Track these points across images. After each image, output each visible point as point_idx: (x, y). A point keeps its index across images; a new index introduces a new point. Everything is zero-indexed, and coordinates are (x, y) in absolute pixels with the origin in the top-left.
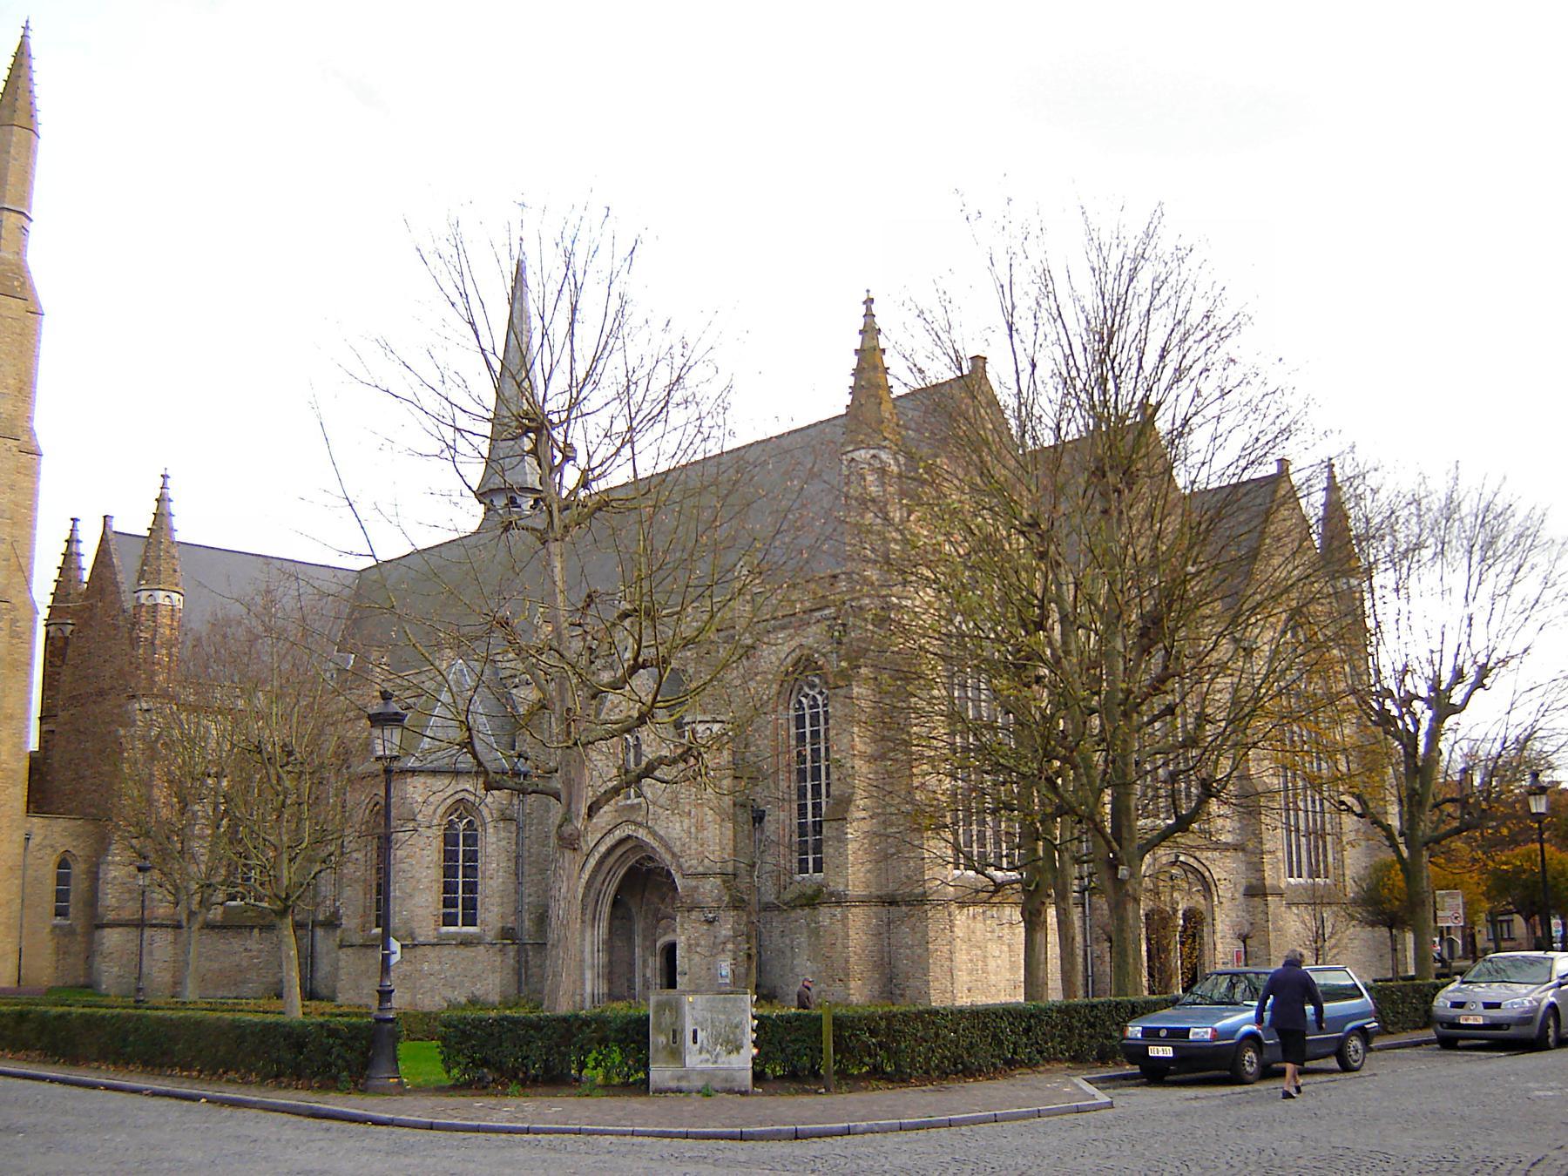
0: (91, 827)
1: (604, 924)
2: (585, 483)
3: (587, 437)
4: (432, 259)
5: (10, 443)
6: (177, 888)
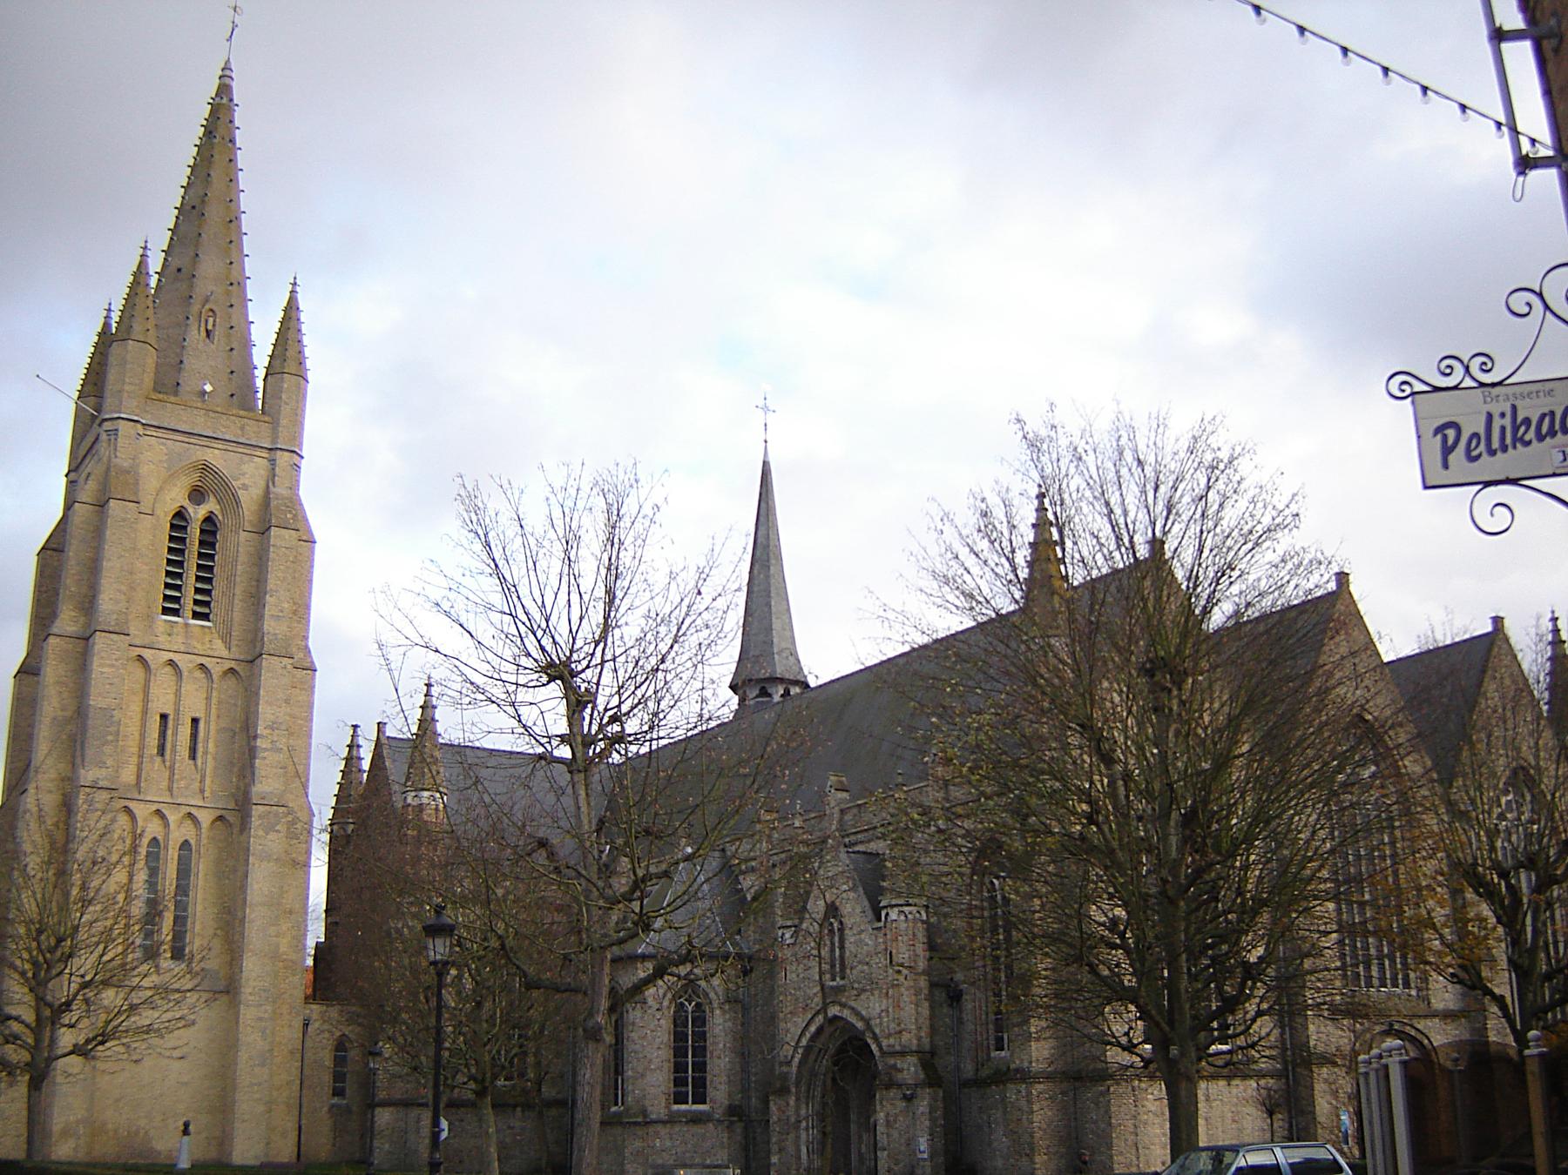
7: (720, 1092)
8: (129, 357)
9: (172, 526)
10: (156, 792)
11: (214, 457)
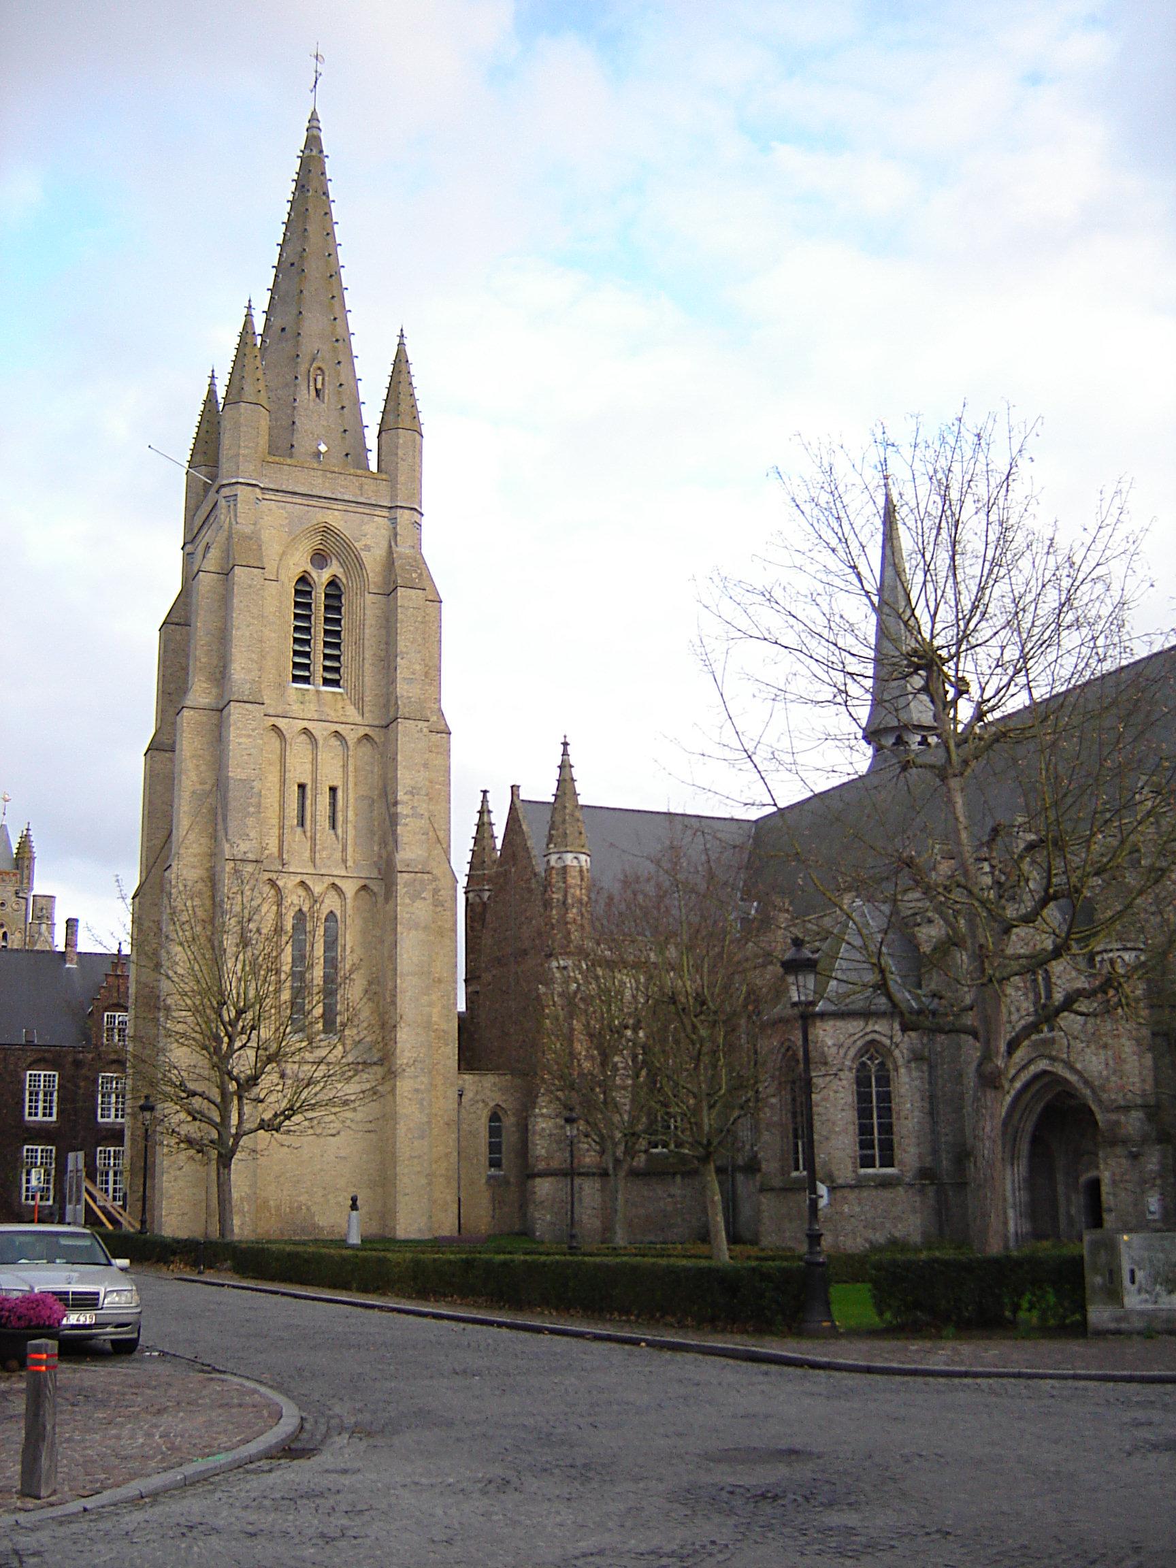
0: (518, 1081)
1: (1024, 1162)
2: (979, 715)
3: (979, 669)
4: (806, 508)
5: (421, 724)
6: (602, 1136)
7: (909, 1153)
8: (242, 420)
9: (297, 592)
10: (299, 864)
11: (335, 518)
